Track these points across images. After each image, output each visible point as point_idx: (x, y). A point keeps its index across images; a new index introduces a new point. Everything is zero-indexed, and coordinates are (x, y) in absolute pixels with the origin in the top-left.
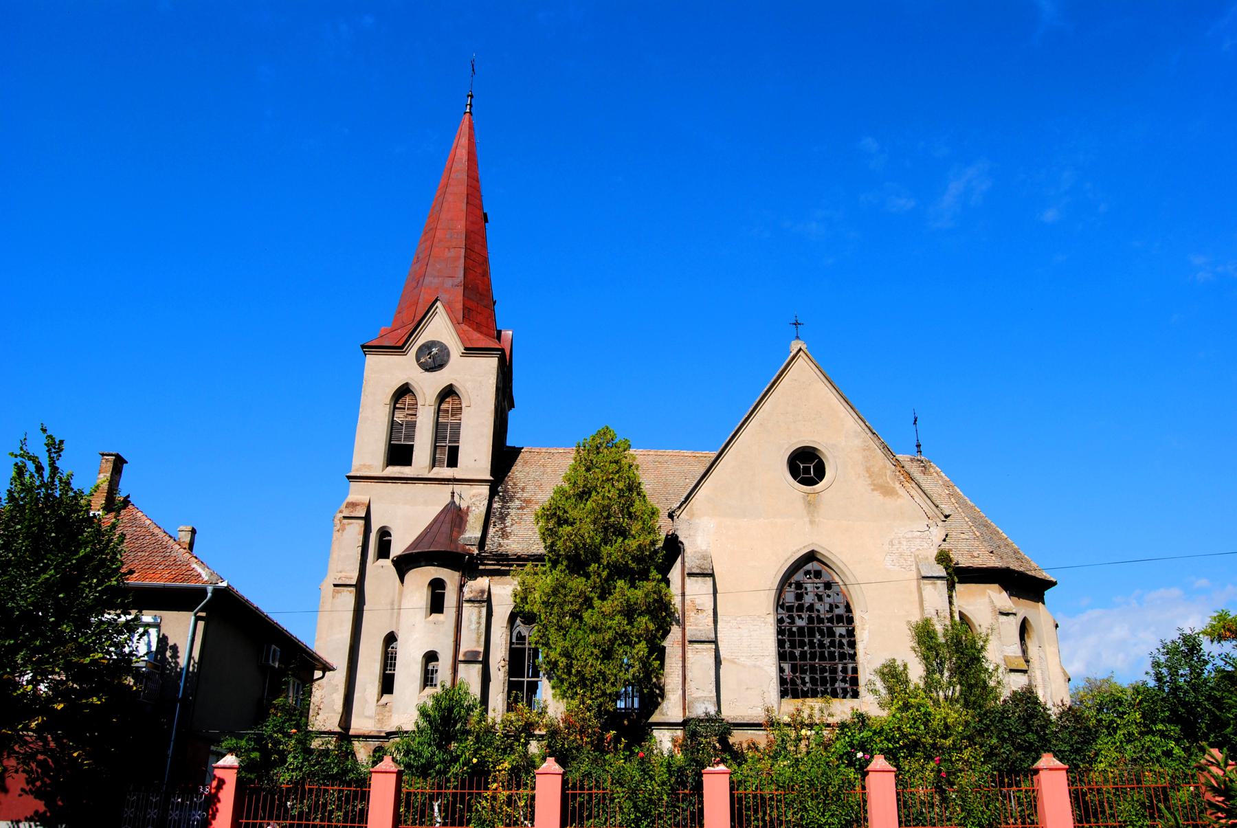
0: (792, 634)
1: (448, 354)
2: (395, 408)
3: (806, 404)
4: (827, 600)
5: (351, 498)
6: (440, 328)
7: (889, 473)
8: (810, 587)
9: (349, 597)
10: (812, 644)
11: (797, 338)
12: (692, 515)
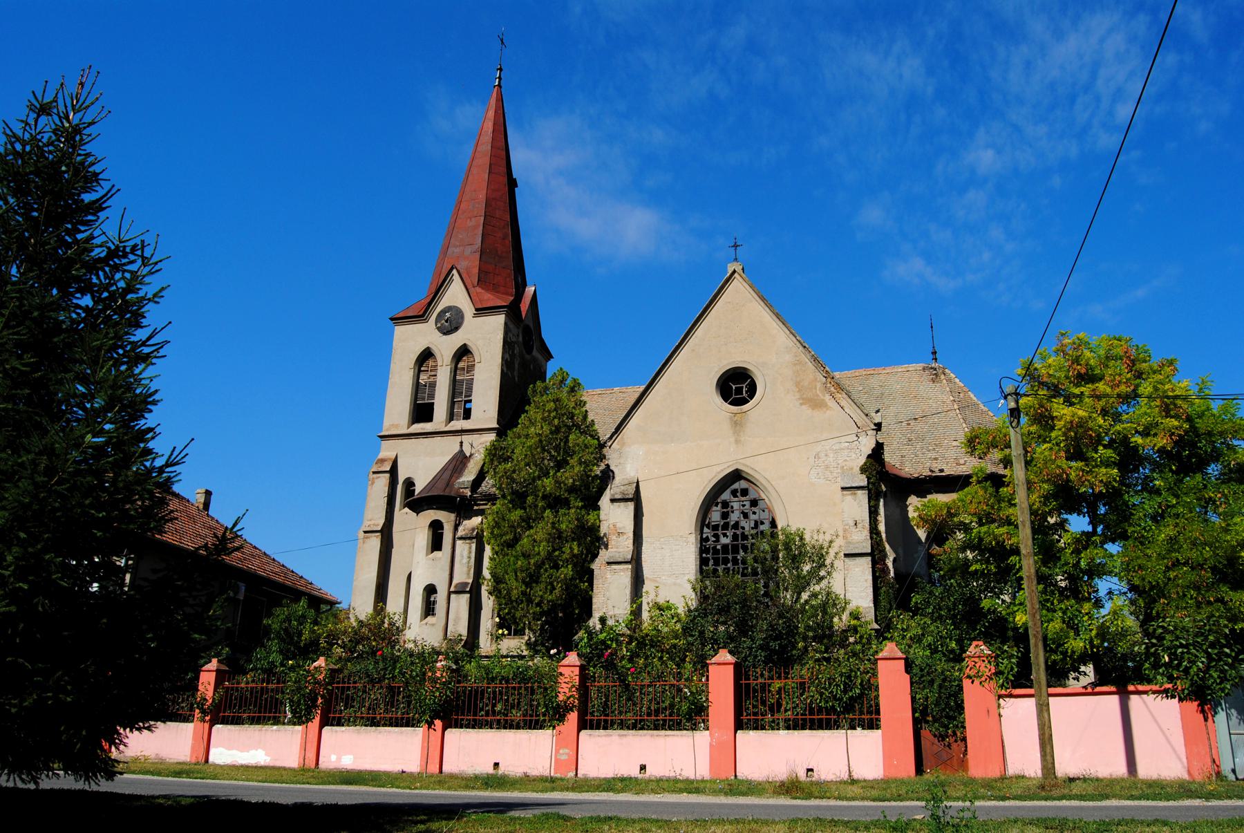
0: (716, 551)
1: (462, 317)
2: (420, 371)
3: (743, 327)
4: (753, 517)
5: (382, 455)
6: (456, 295)
7: (819, 385)
8: (736, 505)
9: (375, 543)
10: (735, 561)
11: (736, 260)
12: (623, 444)
